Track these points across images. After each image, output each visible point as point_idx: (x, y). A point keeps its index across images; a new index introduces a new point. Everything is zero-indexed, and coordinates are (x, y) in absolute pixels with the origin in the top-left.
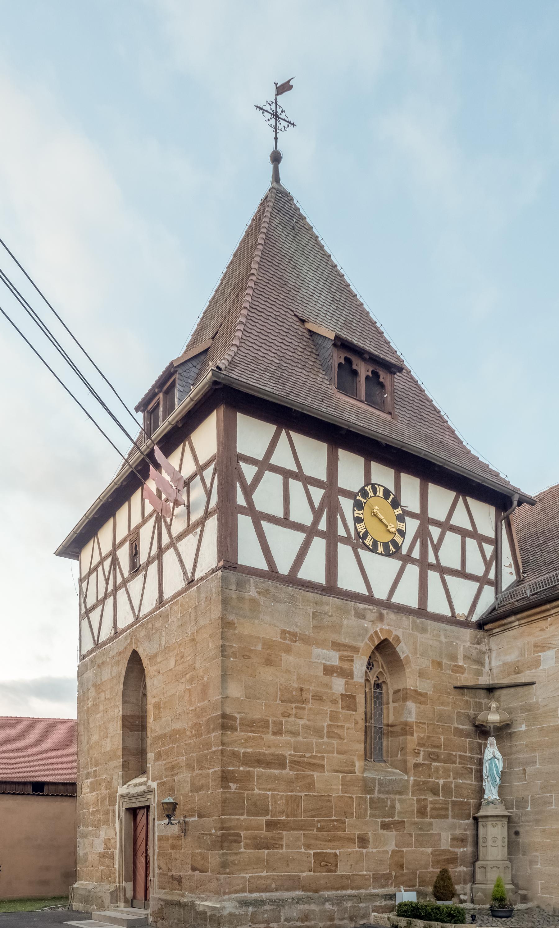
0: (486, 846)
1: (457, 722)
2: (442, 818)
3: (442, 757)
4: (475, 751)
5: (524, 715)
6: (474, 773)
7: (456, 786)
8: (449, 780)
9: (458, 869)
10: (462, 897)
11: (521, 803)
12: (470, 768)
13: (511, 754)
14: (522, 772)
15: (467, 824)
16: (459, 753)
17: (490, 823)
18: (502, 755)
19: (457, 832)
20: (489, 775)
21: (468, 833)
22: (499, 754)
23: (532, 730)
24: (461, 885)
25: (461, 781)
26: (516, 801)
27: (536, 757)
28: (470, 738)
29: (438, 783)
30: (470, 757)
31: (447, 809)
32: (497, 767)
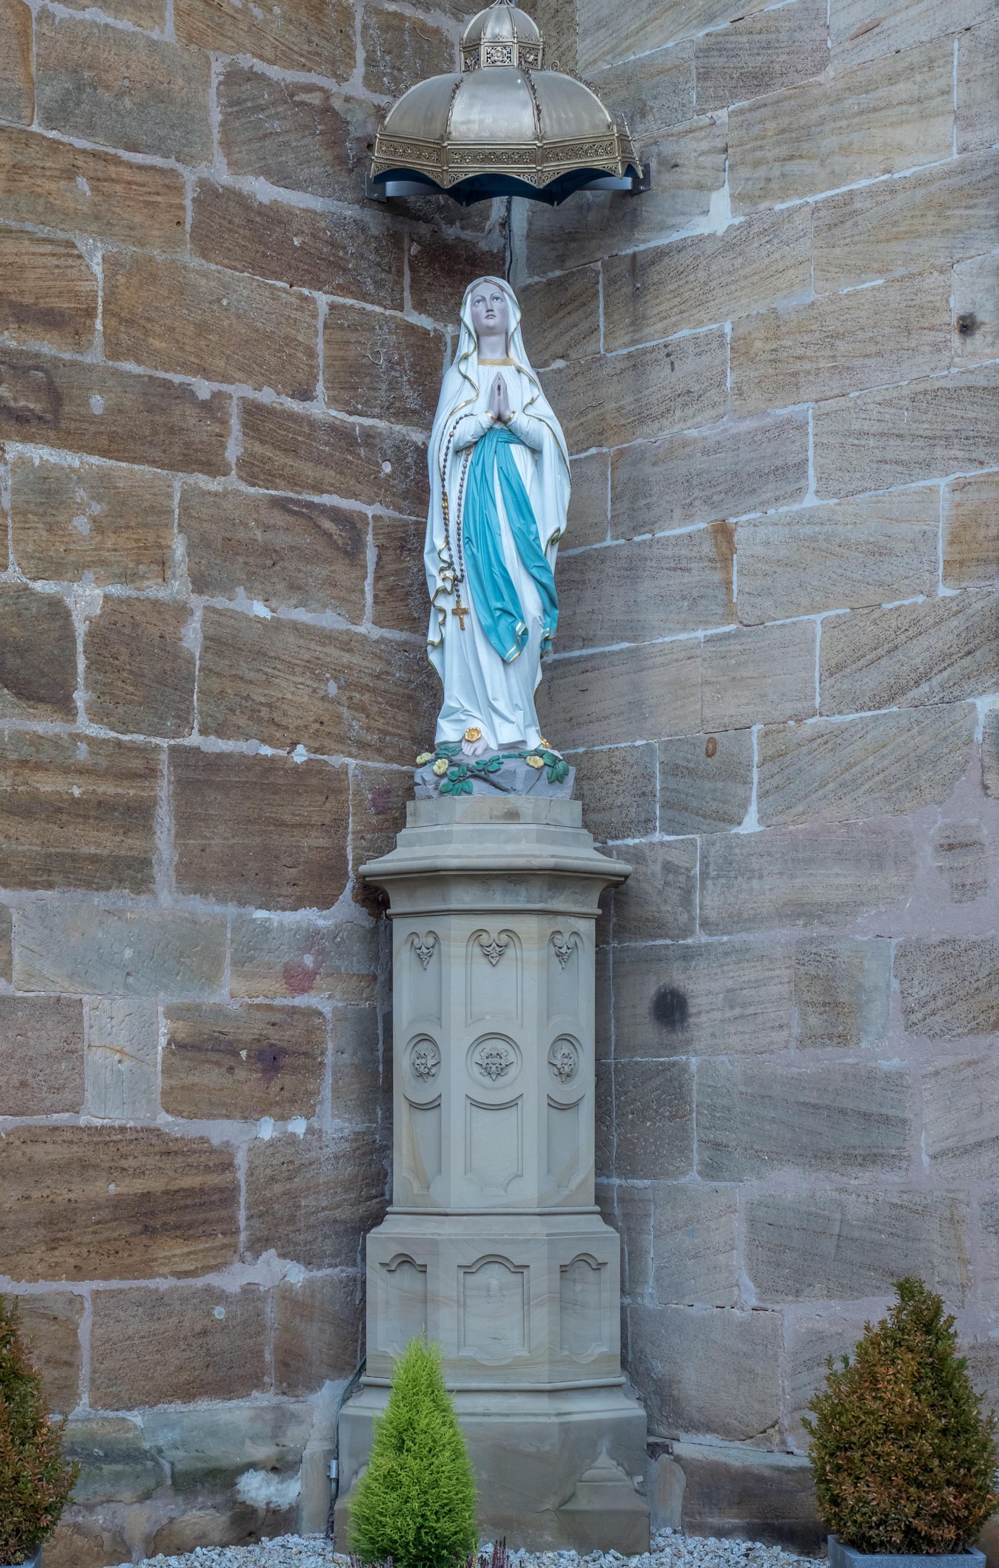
0: (434, 1105)
1: (227, 145)
2: (88, 884)
3: (97, 403)
4: (383, 394)
5: (722, 115)
6: (371, 555)
7: (214, 643)
8: (154, 590)
9: (232, 1279)
10: (257, 1489)
11: (700, 781)
12: (336, 515)
13: (641, 418)
14: (707, 548)
15: (311, 939)
16: (241, 391)
17: (459, 927)
18: (561, 415)
19: (230, 994)
20: (463, 566)
21: (322, 1001)
22: (543, 407)
23: (773, 229)
24: (264, 1399)
25: (260, 610)
26: (672, 770)
27: (801, 427)
28: (342, 290)
29: (57, 610)
30: (335, 430)
31: (137, 815)
32: (521, 506)
